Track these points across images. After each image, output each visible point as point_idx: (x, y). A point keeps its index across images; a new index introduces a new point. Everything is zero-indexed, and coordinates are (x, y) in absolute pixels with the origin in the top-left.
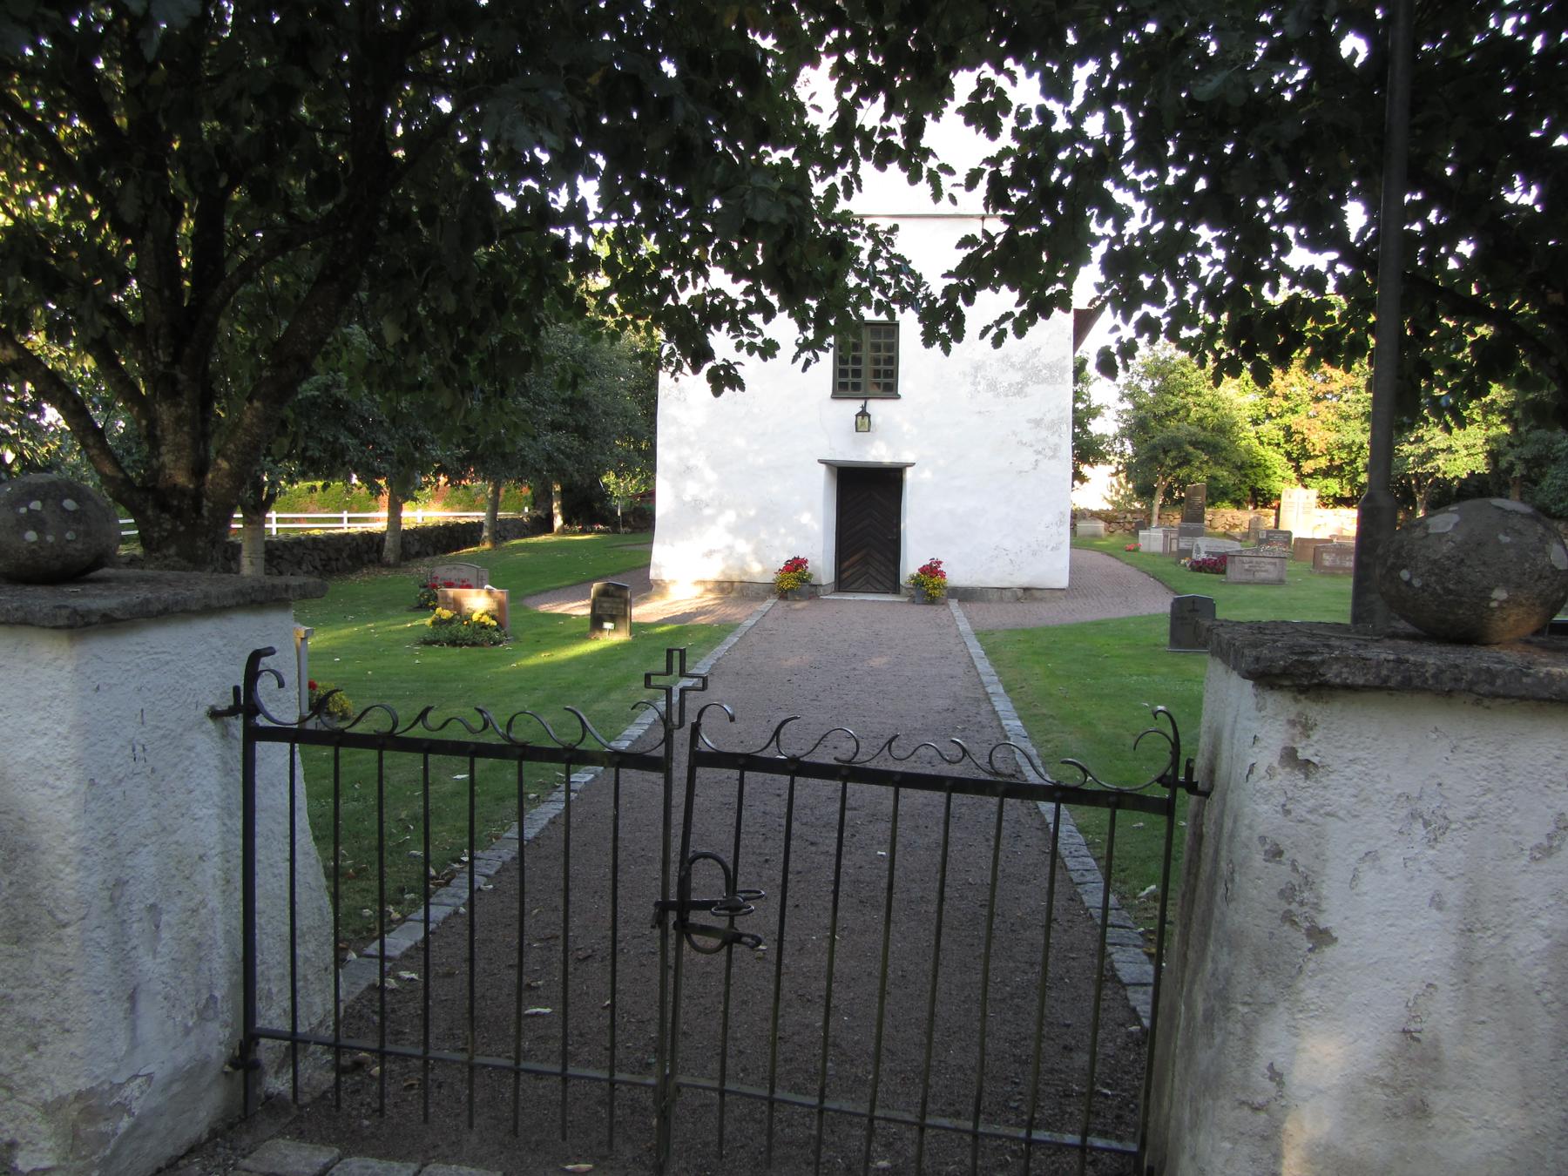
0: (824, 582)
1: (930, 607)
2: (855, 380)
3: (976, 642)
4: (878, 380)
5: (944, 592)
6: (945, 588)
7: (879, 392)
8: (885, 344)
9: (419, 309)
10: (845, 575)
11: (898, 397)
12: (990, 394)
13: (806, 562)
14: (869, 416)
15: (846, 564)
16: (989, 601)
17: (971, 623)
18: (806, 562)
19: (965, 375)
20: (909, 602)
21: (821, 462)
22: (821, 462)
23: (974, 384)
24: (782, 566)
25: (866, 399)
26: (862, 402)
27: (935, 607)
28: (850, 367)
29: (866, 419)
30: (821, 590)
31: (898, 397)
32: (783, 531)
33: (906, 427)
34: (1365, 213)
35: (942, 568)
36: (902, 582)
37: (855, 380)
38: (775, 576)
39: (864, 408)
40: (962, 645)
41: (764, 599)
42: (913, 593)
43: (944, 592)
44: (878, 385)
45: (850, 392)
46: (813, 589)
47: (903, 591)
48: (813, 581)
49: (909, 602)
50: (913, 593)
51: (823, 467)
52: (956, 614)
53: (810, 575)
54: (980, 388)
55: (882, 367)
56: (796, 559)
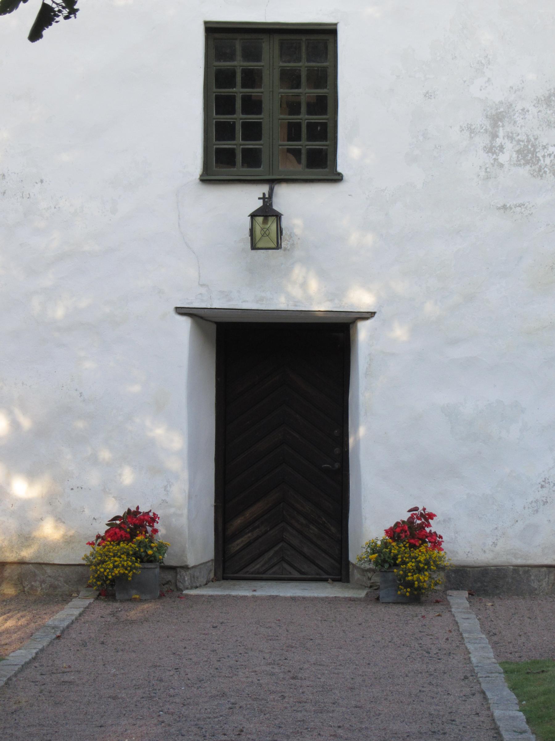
0: (191, 561)
1: (411, 609)
2: (251, 145)
3: (507, 693)
4: (294, 145)
5: (440, 577)
6: (443, 568)
7: (299, 169)
8: (310, 71)
9: (138, 573)
10: (237, 545)
11: (337, 178)
12: (524, 171)
13: (153, 519)
14: (278, 216)
15: (238, 522)
16: (532, 593)
17: (495, 645)
18: (153, 519)
19: (471, 130)
20: (367, 600)
21: (181, 311)
22: (181, 311)
23: (490, 150)
24: (102, 529)
25: (272, 182)
26: (264, 189)
27: (420, 610)
28: (304, 118)
29: (272, 220)
30: (187, 577)
31: (337, 178)
32: (105, 455)
33: (354, 238)
34: (47, 27)
35: (435, 527)
36: (353, 558)
37: (251, 145)
38: (89, 550)
39: (267, 200)
40: (478, 698)
41: (66, 598)
42: (376, 579)
43: (440, 577)
44: (296, 153)
45: (240, 170)
46: (169, 576)
47: (356, 575)
48: (169, 560)
49: (367, 600)
50: (376, 579)
51: (186, 323)
52: (464, 625)
53: (162, 548)
54: (503, 158)
55: (304, 118)
56: (157, 530)
